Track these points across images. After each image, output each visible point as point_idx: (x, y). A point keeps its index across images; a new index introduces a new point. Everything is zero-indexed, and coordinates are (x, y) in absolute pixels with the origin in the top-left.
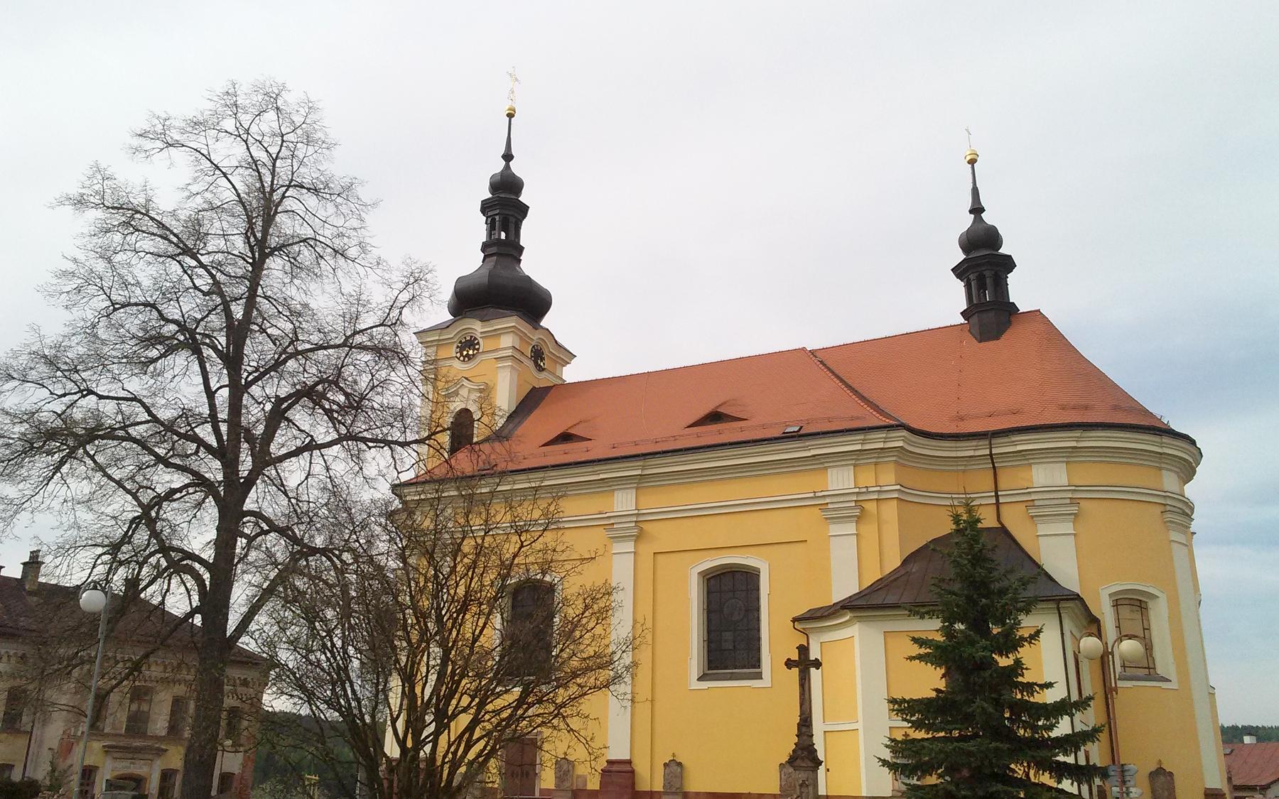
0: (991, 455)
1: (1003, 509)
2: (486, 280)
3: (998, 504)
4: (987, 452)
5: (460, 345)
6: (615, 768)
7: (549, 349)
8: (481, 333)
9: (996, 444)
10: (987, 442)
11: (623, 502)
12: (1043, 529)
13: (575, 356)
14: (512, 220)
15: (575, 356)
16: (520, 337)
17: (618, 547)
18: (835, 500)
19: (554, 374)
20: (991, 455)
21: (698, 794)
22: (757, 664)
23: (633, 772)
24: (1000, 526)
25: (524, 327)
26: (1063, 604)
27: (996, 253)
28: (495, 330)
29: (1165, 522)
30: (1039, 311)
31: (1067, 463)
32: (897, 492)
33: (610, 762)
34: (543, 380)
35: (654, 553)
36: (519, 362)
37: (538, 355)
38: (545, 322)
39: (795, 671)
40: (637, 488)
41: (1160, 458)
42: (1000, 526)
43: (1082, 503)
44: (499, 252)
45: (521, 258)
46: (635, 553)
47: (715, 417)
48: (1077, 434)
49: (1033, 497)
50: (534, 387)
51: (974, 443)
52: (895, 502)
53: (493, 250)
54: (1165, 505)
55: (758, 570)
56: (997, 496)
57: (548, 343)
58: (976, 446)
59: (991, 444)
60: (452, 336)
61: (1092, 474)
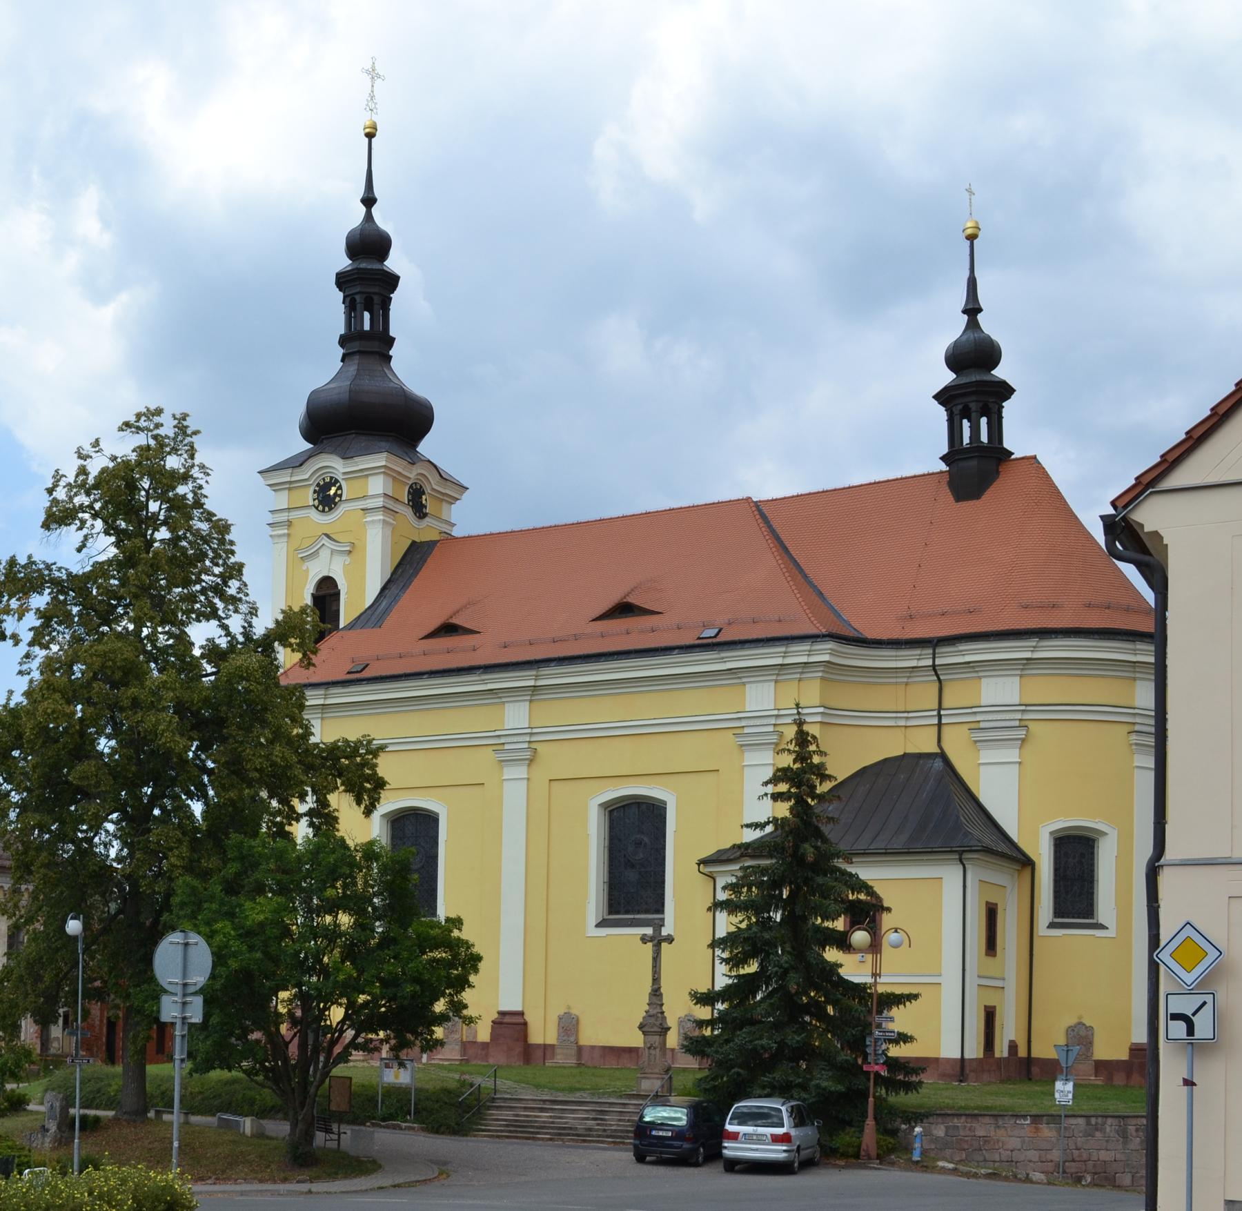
0: (934, 666)
1: (945, 730)
2: (347, 396)
3: (940, 725)
4: (930, 662)
5: (317, 489)
6: (507, 1019)
7: (432, 484)
8: (344, 473)
9: (939, 653)
10: (931, 651)
11: (516, 716)
12: (987, 756)
13: (467, 489)
14: (377, 299)
15: (467, 489)
16: (394, 478)
17: (511, 772)
18: (751, 722)
19: (439, 519)
20: (934, 666)
21: (593, 1047)
22: (660, 909)
23: (525, 1024)
24: (939, 751)
25: (399, 465)
26: (966, 856)
27: (986, 378)
28: (361, 470)
29: (1131, 745)
30: (1035, 457)
31: (1021, 676)
32: (820, 715)
33: (502, 1014)
34: (425, 531)
35: (550, 780)
36: (392, 513)
37: (416, 500)
38: (426, 447)
39: (650, 945)
40: (531, 701)
41: (1134, 667)
42: (939, 751)
43: (1031, 725)
44: (362, 349)
45: (391, 353)
46: (528, 779)
47: (624, 609)
48: (1032, 642)
49: (978, 718)
50: (414, 543)
51: (918, 652)
52: (818, 726)
53: (356, 346)
54: (1134, 724)
55: (665, 803)
56: (940, 716)
57: (430, 479)
58: (920, 655)
59: (934, 654)
60: (306, 476)
61: (1048, 689)
